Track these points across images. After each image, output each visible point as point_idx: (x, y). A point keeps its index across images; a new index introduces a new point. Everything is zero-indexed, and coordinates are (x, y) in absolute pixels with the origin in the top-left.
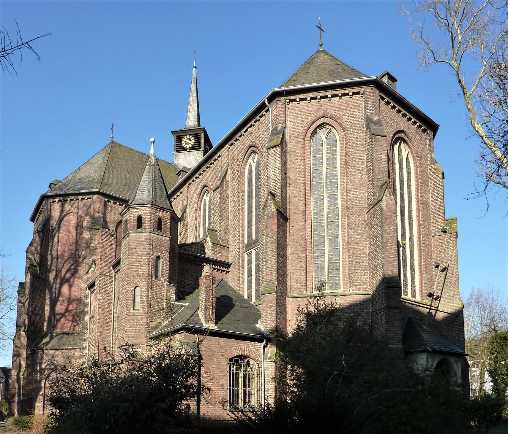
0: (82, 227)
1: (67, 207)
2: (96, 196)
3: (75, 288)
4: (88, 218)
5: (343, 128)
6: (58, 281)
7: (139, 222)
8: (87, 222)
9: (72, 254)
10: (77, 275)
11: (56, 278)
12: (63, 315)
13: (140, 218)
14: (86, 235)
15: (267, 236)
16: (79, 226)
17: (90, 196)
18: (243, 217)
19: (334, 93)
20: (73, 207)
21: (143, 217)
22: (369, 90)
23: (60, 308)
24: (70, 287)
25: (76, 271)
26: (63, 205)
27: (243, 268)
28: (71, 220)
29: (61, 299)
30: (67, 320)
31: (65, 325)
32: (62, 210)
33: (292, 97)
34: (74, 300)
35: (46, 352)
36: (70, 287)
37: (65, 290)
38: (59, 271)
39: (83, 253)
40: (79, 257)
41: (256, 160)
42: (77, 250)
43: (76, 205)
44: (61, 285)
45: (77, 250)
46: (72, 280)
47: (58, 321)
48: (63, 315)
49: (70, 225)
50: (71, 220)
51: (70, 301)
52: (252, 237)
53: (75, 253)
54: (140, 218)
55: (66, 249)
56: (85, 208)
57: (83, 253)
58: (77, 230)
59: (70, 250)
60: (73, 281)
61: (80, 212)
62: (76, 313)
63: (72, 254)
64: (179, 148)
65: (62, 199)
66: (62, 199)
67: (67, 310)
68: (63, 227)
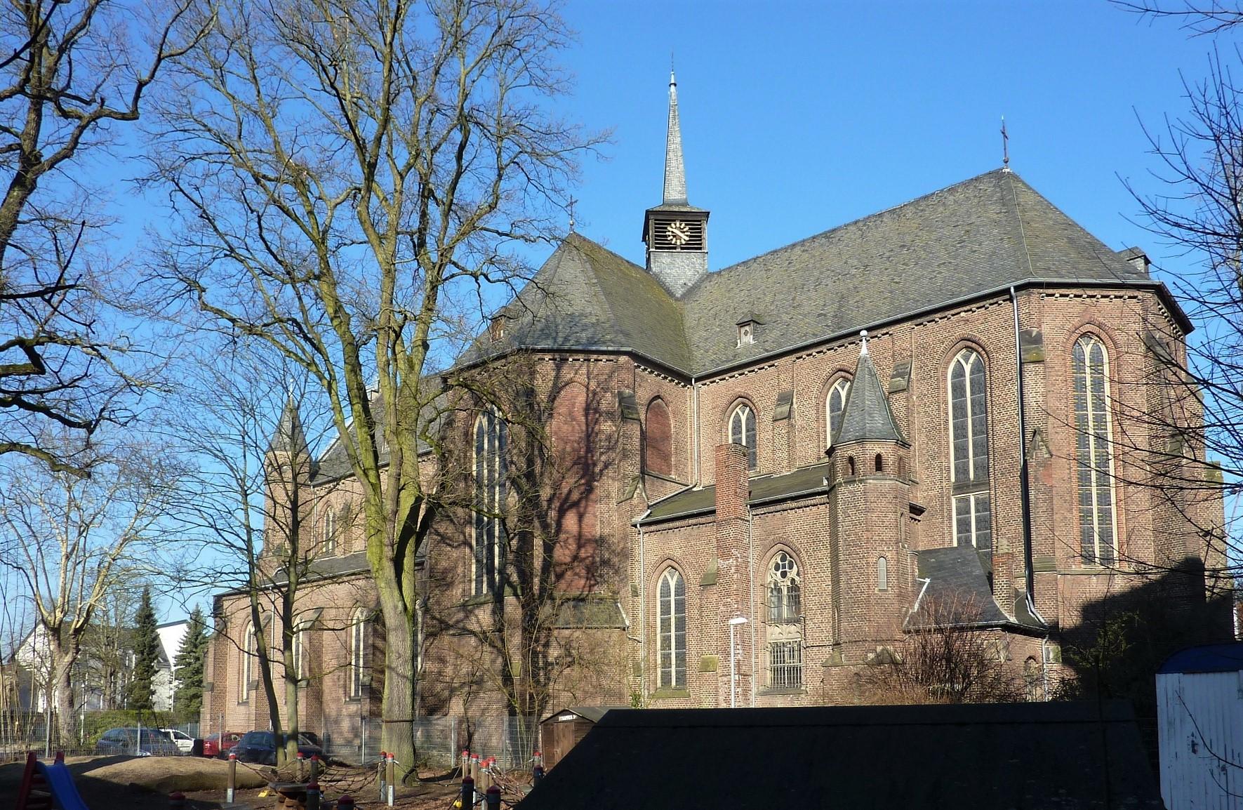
0: (596, 411)
1: (567, 373)
2: (623, 359)
3: (588, 519)
4: (608, 395)
5: (1115, 344)
6: (556, 504)
7: (879, 462)
8: (608, 402)
9: (579, 458)
10: (592, 497)
11: (550, 501)
12: (569, 566)
13: (879, 457)
14: (607, 427)
15: (1038, 490)
16: (591, 409)
17: (612, 357)
18: (948, 443)
19: (1105, 293)
20: (578, 373)
21: (884, 456)
22: (1150, 298)
23: (562, 554)
24: (581, 517)
25: (590, 490)
26: (558, 368)
27: (950, 518)
28: (575, 397)
29: (563, 536)
30: (576, 574)
31: (575, 584)
32: (557, 377)
33: (1050, 291)
34: (589, 541)
35: (555, 633)
36: (581, 517)
37: (570, 521)
38: (556, 486)
39: (603, 458)
40: (595, 465)
41: (971, 360)
42: (589, 450)
43: (584, 370)
44: (562, 513)
45: (589, 450)
46: (583, 504)
47: (559, 577)
48: (569, 566)
49: (573, 405)
50: (575, 397)
51: (581, 541)
52: (966, 472)
53: (586, 457)
54: (879, 457)
55: (568, 449)
56: (602, 378)
57: (603, 458)
58: (586, 415)
59: (574, 450)
60: (586, 507)
61: (593, 385)
62: (593, 563)
63: (579, 458)
64: (663, 244)
65: (557, 356)
66: (557, 356)
67: (575, 558)
68: (561, 406)
